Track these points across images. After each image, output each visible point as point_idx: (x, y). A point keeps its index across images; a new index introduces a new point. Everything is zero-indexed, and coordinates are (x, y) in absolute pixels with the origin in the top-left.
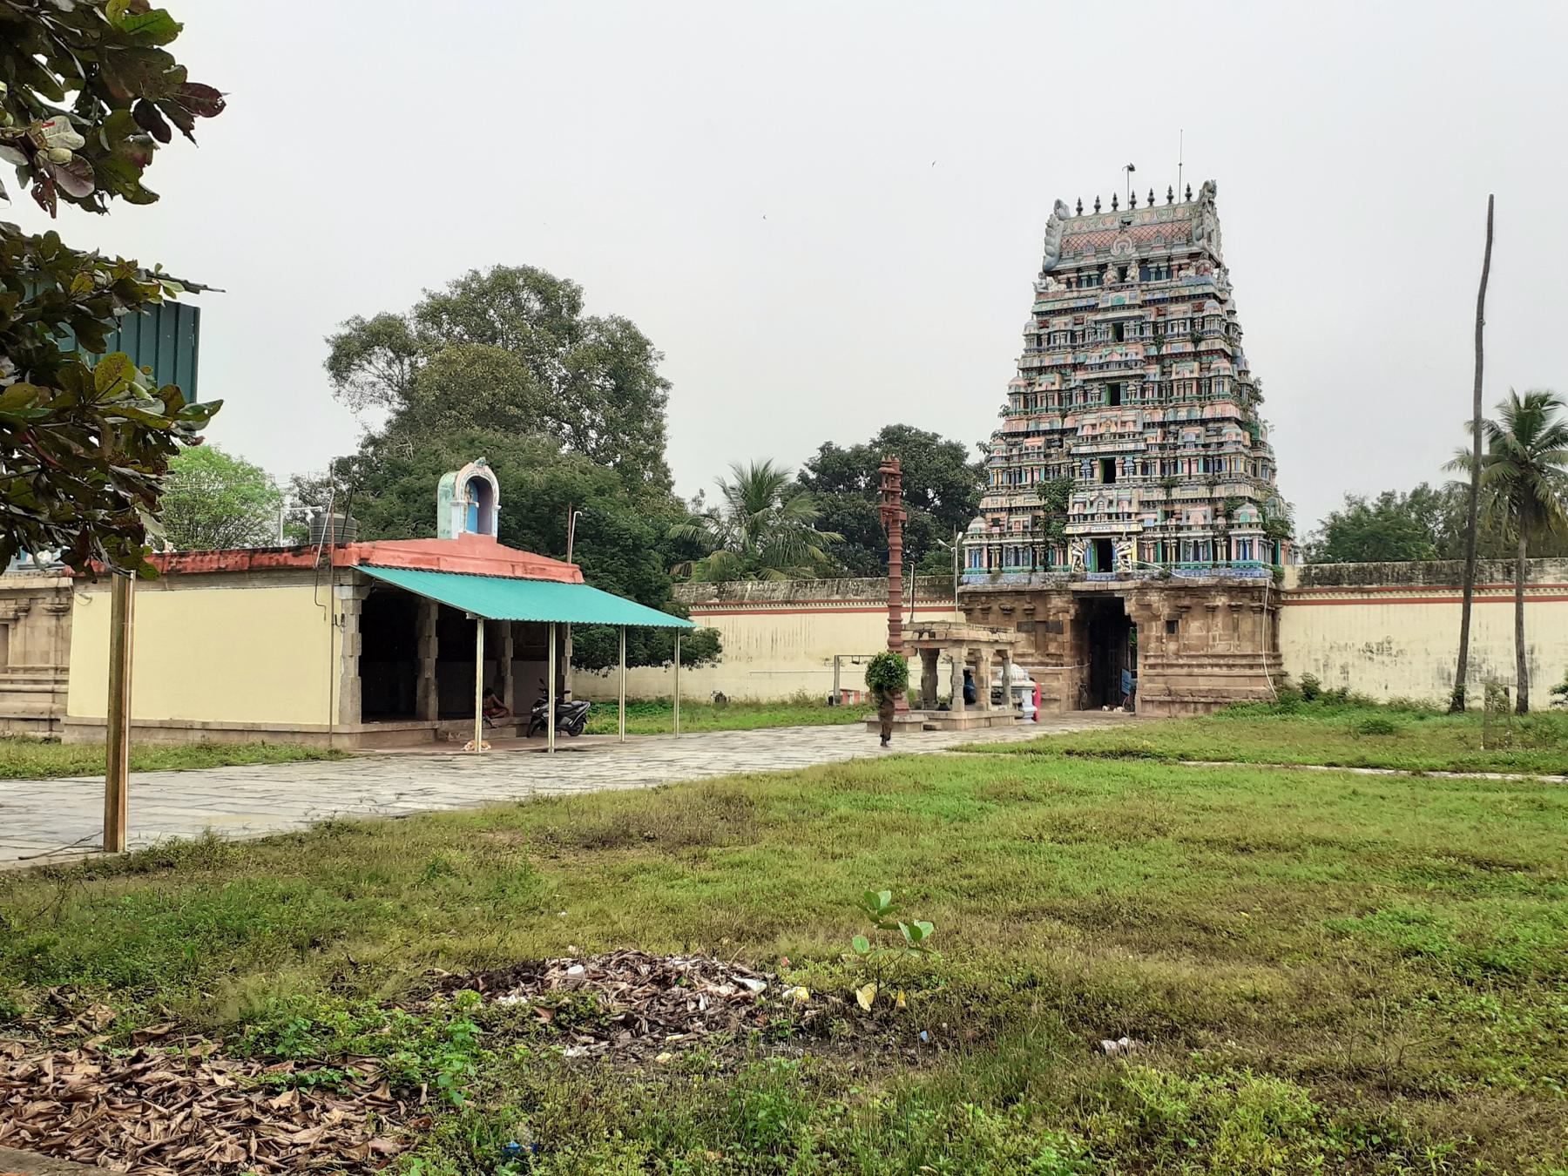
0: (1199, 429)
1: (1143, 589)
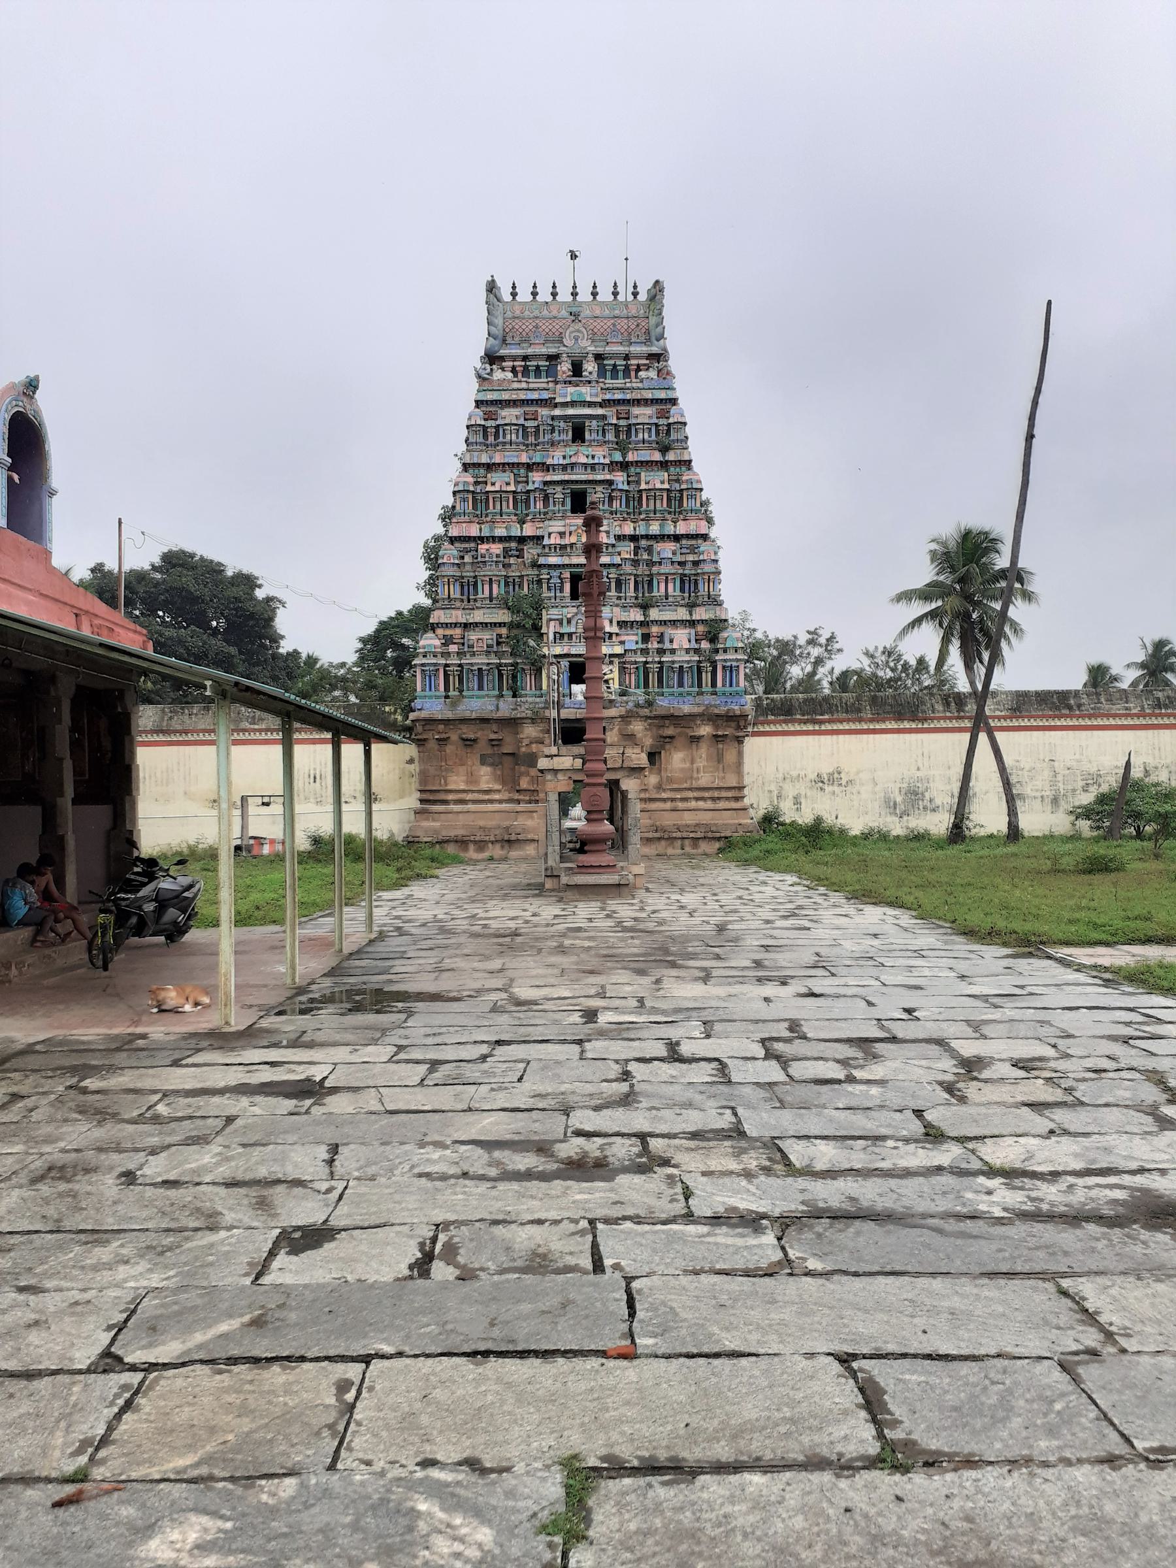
1: (626, 718)
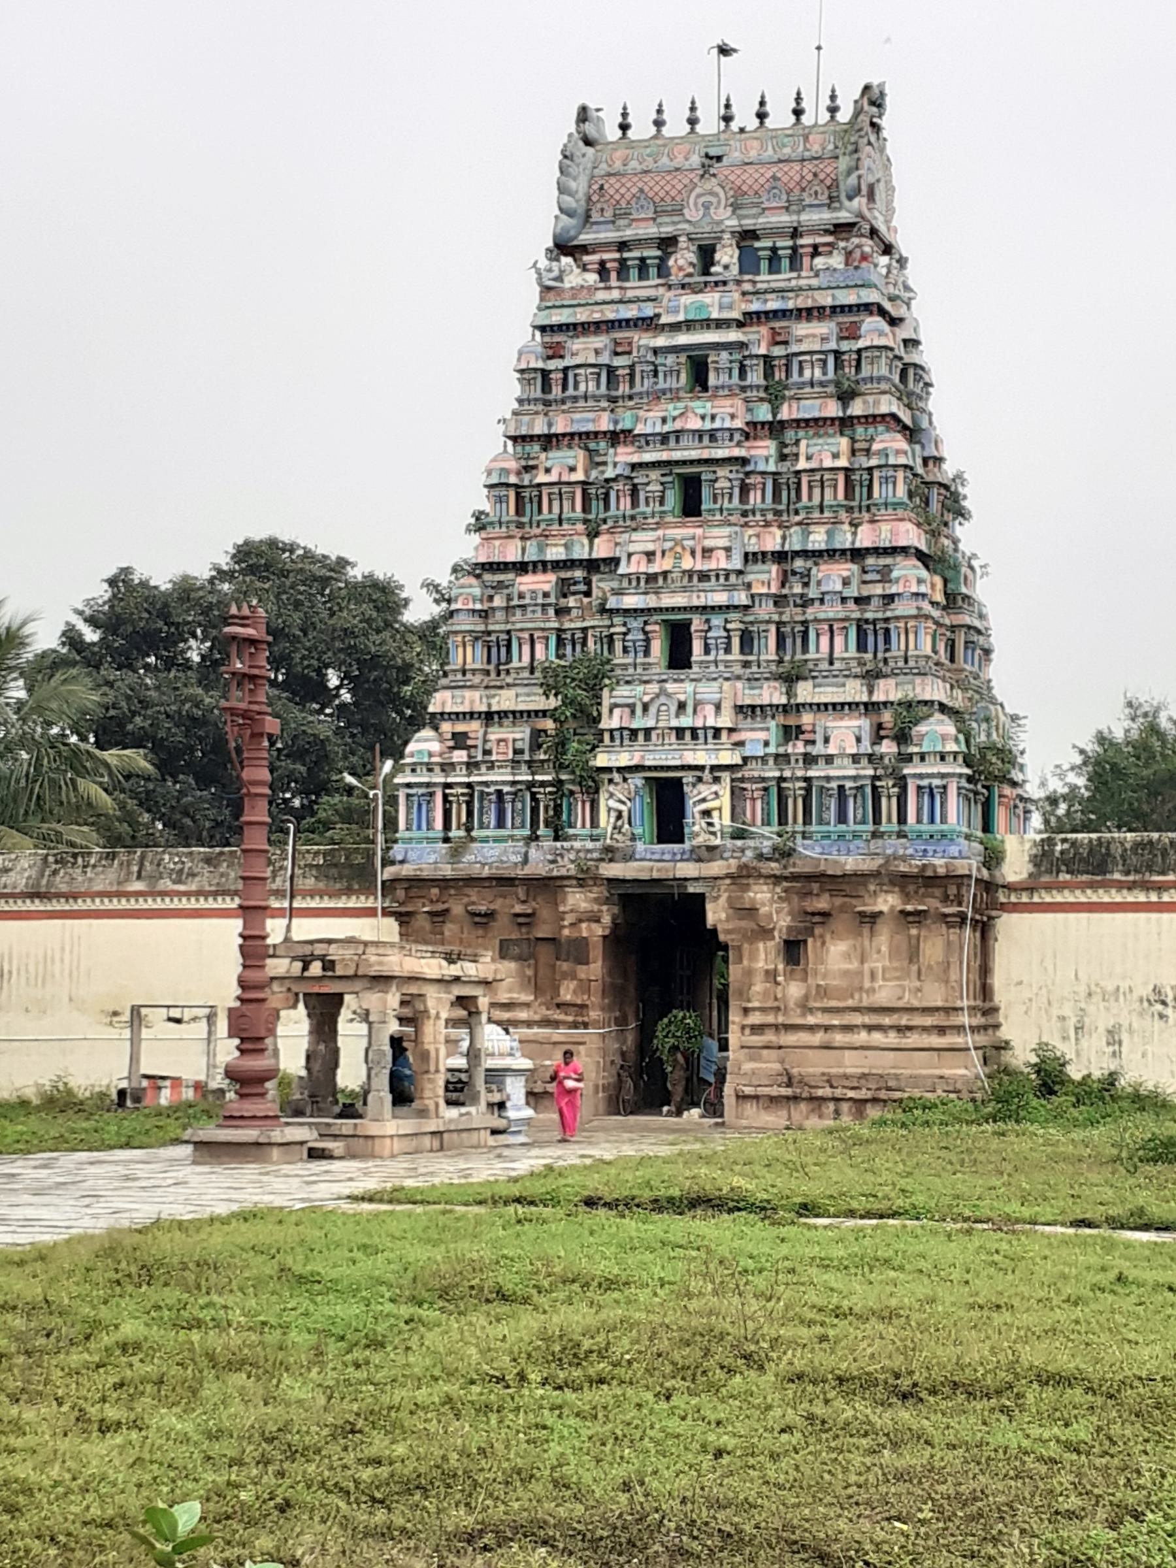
0: (848, 569)
1: (742, 877)
